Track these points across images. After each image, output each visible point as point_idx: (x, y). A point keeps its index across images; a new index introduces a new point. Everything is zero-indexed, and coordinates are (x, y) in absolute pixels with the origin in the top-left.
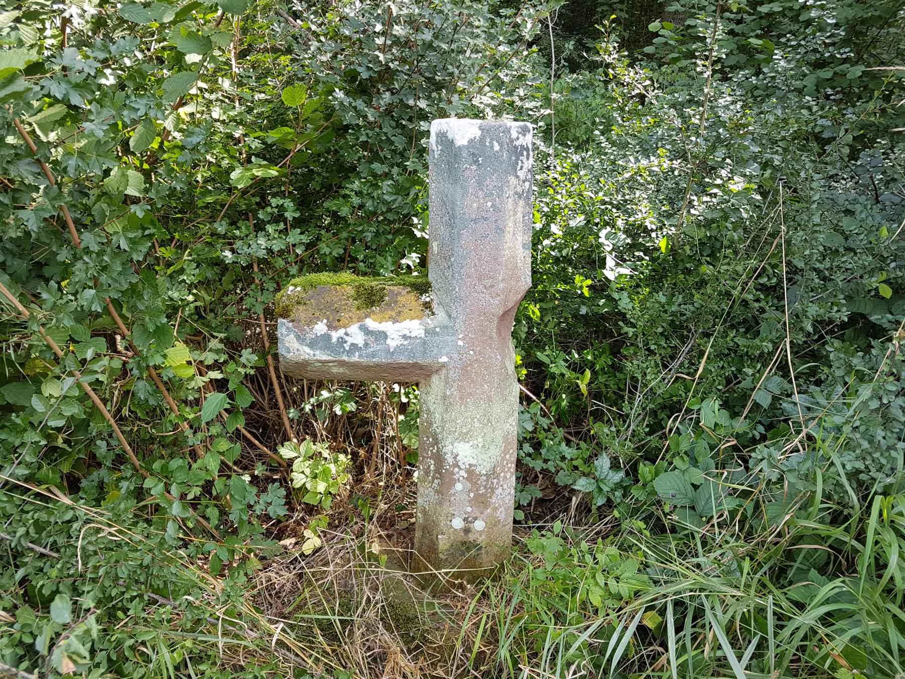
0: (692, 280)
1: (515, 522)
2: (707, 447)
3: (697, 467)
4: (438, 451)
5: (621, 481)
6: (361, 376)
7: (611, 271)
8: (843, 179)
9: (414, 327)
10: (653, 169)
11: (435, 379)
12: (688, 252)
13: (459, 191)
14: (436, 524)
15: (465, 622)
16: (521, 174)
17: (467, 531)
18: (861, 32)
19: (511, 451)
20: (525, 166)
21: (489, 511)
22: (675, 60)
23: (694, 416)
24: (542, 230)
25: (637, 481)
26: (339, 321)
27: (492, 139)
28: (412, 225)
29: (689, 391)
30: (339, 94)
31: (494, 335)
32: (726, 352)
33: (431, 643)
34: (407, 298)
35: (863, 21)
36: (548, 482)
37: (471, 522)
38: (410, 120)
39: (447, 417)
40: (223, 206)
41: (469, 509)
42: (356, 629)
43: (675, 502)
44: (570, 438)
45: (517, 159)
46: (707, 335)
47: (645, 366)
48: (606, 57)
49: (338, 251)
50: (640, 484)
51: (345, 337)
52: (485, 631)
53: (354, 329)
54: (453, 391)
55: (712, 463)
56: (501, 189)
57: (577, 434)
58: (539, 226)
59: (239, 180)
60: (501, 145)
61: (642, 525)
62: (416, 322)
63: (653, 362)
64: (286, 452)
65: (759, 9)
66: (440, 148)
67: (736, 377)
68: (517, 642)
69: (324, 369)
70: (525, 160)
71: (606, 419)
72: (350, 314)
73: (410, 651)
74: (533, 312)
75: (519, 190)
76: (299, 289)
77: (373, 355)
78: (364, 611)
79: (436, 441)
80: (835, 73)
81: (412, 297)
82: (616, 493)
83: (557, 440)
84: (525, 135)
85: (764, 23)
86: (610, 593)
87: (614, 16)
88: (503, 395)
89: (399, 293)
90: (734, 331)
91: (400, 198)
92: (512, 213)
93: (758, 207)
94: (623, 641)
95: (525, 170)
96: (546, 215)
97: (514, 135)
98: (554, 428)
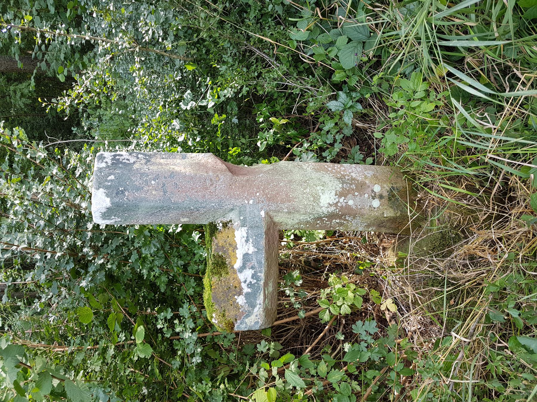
0: (213, 49)
1: (373, 164)
2: (322, 35)
3: (336, 41)
4: (326, 217)
5: (346, 93)
6: (275, 269)
10: (141, 74)
11: (276, 219)
12: (195, 51)
14: (376, 218)
15: (445, 198)
16: (132, 160)
17: (381, 197)
19: (326, 167)
20: (127, 157)
21: (367, 182)
23: (301, 44)
24: (182, 147)
25: (345, 82)
26: (236, 287)
28: (174, 232)
29: (285, 48)
31: (246, 178)
32: (259, 25)
33: (460, 222)
34: (220, 239)
36: (345, 143)
37: (375, 194)
39: (302, 211)
40: (161, 362)
41: (366, 195)
42: (452, 276)
43: (360, 55)
44: (316, 128)
45: (121, 163)
46: (248, 38)
47: (268, 79)
48: (67, 105)
49: (192, 283)
50: (346, 79)
51: (247, 283)
52: (451, 185)
53: (241, 277)
54: (285, 207)
55: (333, 31)
56: (142, 174)
57: (314, 124)
58: (179, 149)
60: (110, 174)
61: (375, 78)
62: (237, 233)
63: (266, 74)
64: (326, 317)
66: (113, 217)
67: (276, 18)
68: (464, 163)
69: (270, 297)
70: (122, 158)
71: (304, 105)
72: (231, 279)
73: (466, 237)
74: (235, 152)
75: (143, 161)
76: (214, 315)
77: (259, 263)
78: (438, 269)
79: (320, 218)
81: (219, 236)
82: (353, 96)
83: (318, 137)
84: (105, 158)
86: (425, 97)
87: (39, 99)
88: (287, 173)
89: (217, 245)
90: (246, 20)
92: (160, 167)
94: (470, 83)
95: (130, 157)
96: (171, 145)
97: (103, 165)
98: (310, 138)
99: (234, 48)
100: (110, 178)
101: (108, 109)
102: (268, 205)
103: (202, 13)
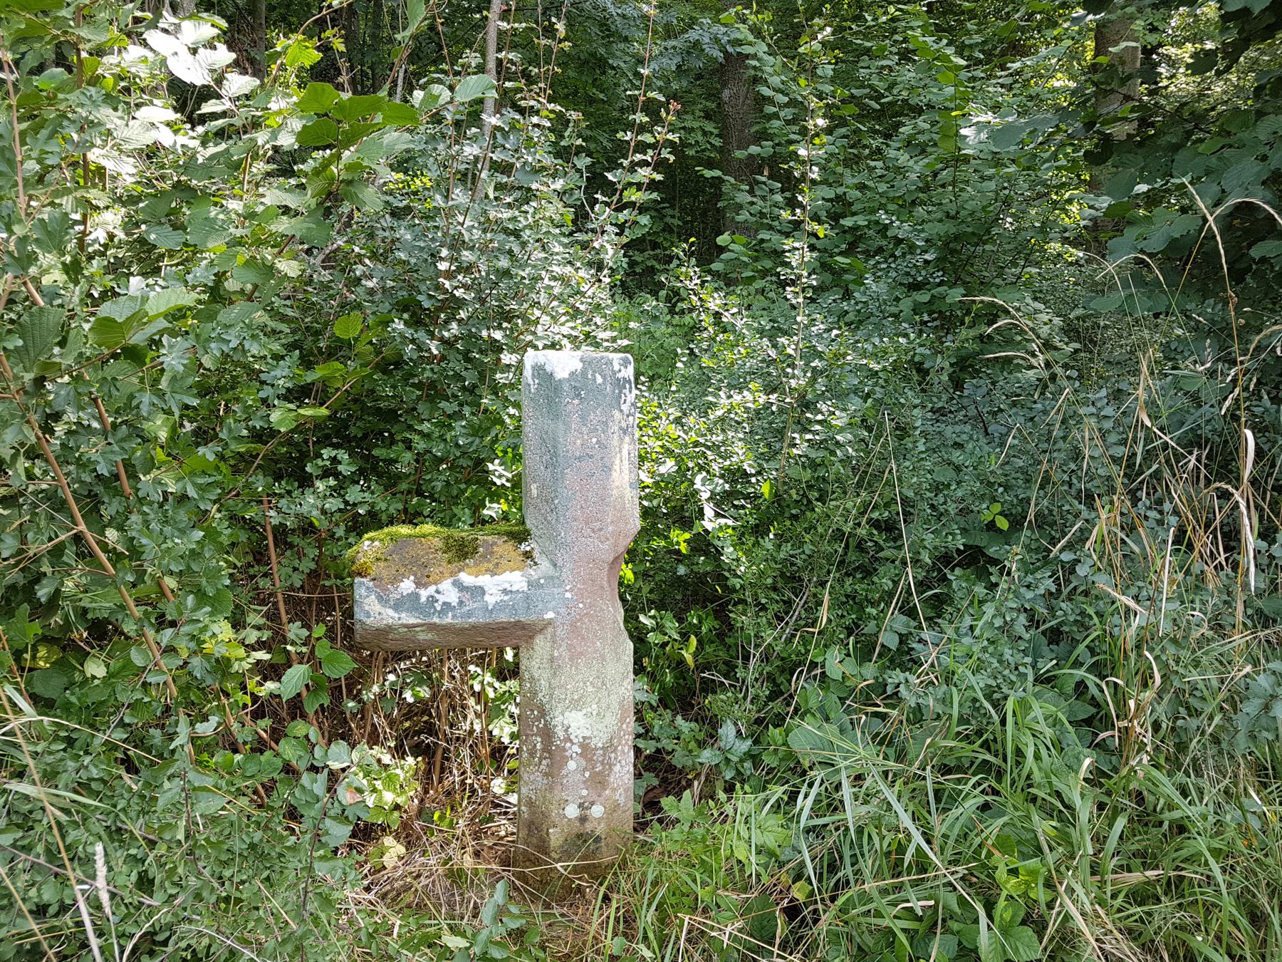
7: (710, 522)
8: (951, 412)
9: (515, 579)
11: (539, 641)
12: (795, 497)
13: (561, 427)
16: (625, 407)
17: (583, 819)
18: (955, 250)
20: (628, 400)
22: (750, 280)
27: (594, 372)
28: (487, 472)
30: (399, 325)
31: (606, 584)
34: (504, 548)
35: (957, 238)
38: (481, 352)
39: (555, 682)
41: (585, 792)
45: (621, 392)
46: (823, 584)
53: (446, 585)
54: (562, 652)
56: (605, 423)
59: (281, 421)
60: (604, 377)
62: (517, 574)
65: (842, 222)
75: (624, 425)
76: (377, 543)
79: (543, 713)
80: (933, 296)
81: (510, 546)
85: (849, 237)
88: (617, 653)
91: (478, 441)
93: (863, 440)
95: (628, 403)
97: (616, 367)
99: (805, 561)
100: (598, 377)
101: (670, 330)
102: (563, 624)
103: (852, 504)
